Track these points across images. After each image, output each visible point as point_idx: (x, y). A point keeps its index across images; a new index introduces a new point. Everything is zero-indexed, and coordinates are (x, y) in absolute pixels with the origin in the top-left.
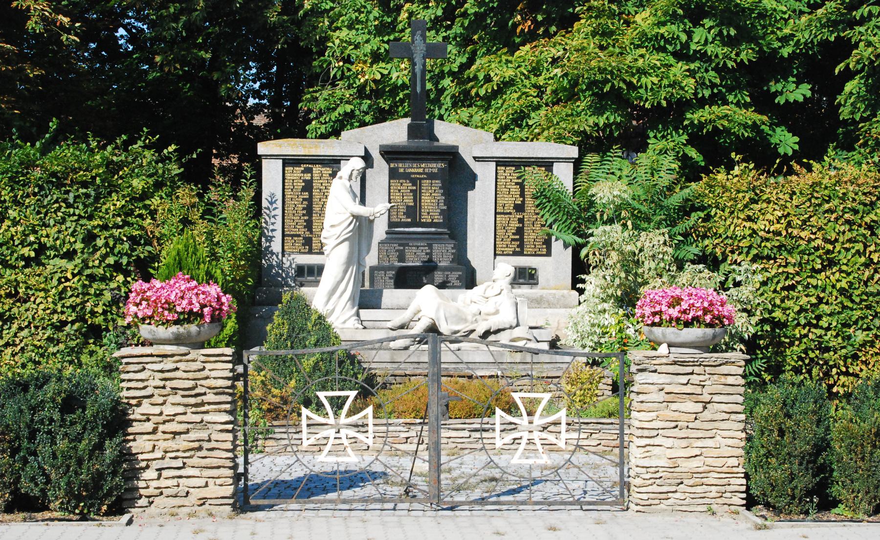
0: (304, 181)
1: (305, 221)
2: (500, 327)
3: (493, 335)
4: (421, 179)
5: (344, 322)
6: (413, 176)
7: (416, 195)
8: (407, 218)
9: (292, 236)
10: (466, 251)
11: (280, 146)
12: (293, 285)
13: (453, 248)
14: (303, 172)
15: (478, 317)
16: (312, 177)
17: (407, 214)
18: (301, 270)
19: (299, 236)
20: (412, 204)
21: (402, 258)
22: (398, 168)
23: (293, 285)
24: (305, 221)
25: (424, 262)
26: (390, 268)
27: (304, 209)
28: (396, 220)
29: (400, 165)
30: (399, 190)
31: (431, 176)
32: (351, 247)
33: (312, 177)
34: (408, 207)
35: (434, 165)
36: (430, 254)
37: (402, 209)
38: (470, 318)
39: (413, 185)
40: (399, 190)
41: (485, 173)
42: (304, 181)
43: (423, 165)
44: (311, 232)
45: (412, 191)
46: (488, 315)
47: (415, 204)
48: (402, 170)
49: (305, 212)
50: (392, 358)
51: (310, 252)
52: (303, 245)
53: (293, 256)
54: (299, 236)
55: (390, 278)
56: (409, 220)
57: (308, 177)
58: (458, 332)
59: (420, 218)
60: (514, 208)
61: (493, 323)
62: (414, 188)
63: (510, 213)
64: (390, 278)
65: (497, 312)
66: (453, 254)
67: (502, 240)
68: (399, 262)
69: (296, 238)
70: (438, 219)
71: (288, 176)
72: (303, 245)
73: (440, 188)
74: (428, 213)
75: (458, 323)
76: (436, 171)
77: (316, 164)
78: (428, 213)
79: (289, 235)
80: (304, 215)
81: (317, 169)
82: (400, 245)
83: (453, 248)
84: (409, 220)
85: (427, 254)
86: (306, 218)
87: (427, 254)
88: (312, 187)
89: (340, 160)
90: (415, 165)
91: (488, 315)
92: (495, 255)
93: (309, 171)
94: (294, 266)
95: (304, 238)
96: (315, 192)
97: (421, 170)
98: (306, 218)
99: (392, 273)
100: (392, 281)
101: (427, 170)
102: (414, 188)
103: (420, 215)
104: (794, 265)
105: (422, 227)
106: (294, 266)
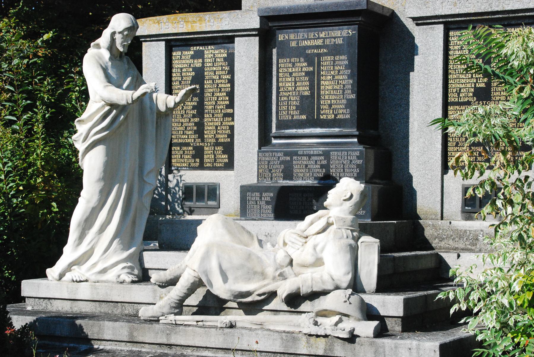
0: (194, 69)
1: (196, 124)
2: (317, 288)
3: (308, 303)
4: (319, 55)
5: (104, 271)
6: (309, 52)
7: (314, 79)
8: (301, 114)
9: (181, 145)
10: (408, 163)
11: (159, 22)
12: (181, 211)
13: (358, 158)
14: (193, 57)
15: (287, 270)
16: (203, 63)
17: (301, 109)
18: (190, 192)
19: (188, 145)
20: (307, 93)
21: (288, 174)
22: (289, 41)
23: (181, 211)
24: (196, 124)
25: (321, 179)
26: (267, 189)
27: (194, 108)
28: (287, 118)
29: (292, 36)
30: (291, 74)
31: (335, 50)
32: (108, 154)
33: (203, 63)
34: (302, 97)
35: (338, 33)
36: (326, 167)
37: (295, 101)
38: (270, 271)
39: (309, 65)
40: (291, 74)
41: (429, 43)
42: (194, 69)
43: (322, 35)
44: (203, 141)
45: (307, 74)
46: (304, 266)
47: (312, 94)
48: (293, 44)
49: (195, 112)
50: (131, 334)
51: (202, 167)
52: (194, 157)
53: (182, 173)
54: (188, 145)
55: (267, 203)
56: (304, 117)
57: (198, 63)
58: (248, 294)
59: (319, 114)
60: (474, 94)
61: (303, 281)
62: (311, 69)
63: (468, 103)
64: (267, 203)
65: (318, 262)
66: (358, 166)
67: (457, 145)
68: (285, 178)
69: (185, 148)
70: (345, 114)
71: (176, 64)
72: (194, 157)
73: (347, 67)
74: (330, 106)
75: (249, 280)
76: (340, 41)
77: (208, 45)
78: (330, 106)
79: (177, 145)
80: (194, 116)
81: (209, 51)
82: (286, 154)
83: (358, 158)
84: (304, 117)
85: (322, 166)
86: (197, 120)
87: (322, 166)
88: (203, 77)
89: (233, 37)
90: (311, 35)
91: (304, 266)
92: (445, 168)
93: (199, 55)
94: (181, 185)
95: (195, 148)
96: (207, 84)
97: (319, 42)
98: (197, 120)
99: (269, 196)
100: (270, 207)
101: (327, 42)
102: (311, 69)
103: (319, 109)
104: (186, 134)
105: (322, 127)
106: (181, 185)
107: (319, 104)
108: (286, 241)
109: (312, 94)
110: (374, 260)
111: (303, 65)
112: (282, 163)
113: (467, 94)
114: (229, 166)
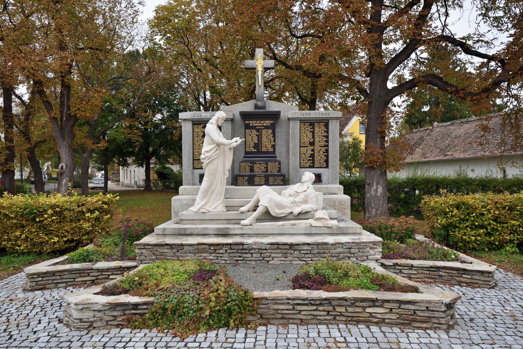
4: (261, 129)
7: (259, 137)
22: (249, 124)
29: (251, 122)
34: (255, 143)
35: (268, 122)
37: (252, 145)
47: (259, 142)
48: (251, 125)
55: (246, 181)
59: (261, 149)
60: (309, 144)
63: (307, 147)
64: (246, 181)
85: (265, 168)
87: (265, 168)
90: (258, 122)
101: (264, 124)
107: (261, 146)
108: (37, 333)
109: (259, 142)
110: (272, 225)
111: (254, 132)
112: (249, 166)
113: (307, 144)
114: (327, 167)
